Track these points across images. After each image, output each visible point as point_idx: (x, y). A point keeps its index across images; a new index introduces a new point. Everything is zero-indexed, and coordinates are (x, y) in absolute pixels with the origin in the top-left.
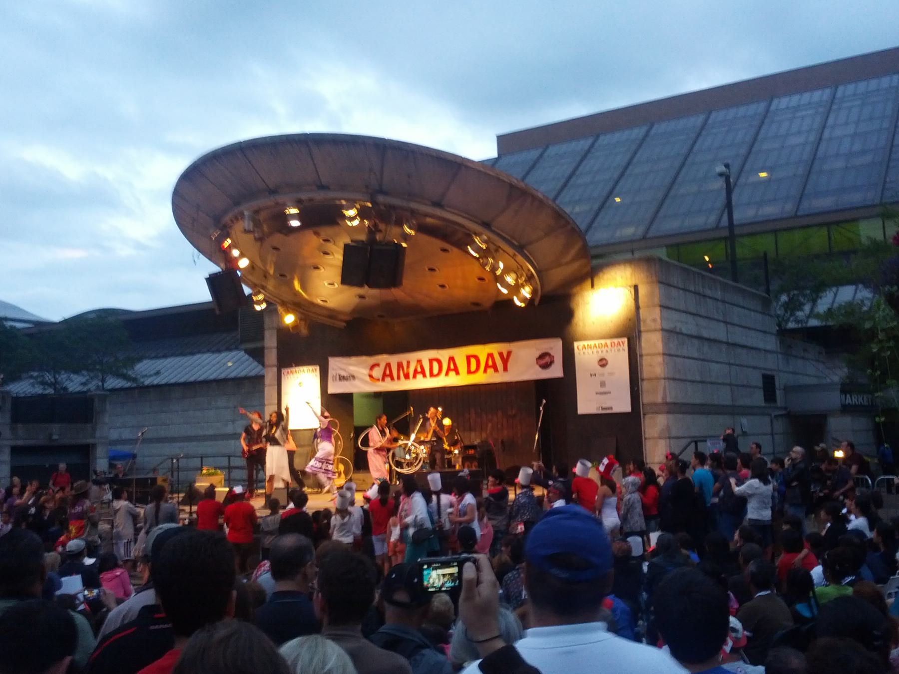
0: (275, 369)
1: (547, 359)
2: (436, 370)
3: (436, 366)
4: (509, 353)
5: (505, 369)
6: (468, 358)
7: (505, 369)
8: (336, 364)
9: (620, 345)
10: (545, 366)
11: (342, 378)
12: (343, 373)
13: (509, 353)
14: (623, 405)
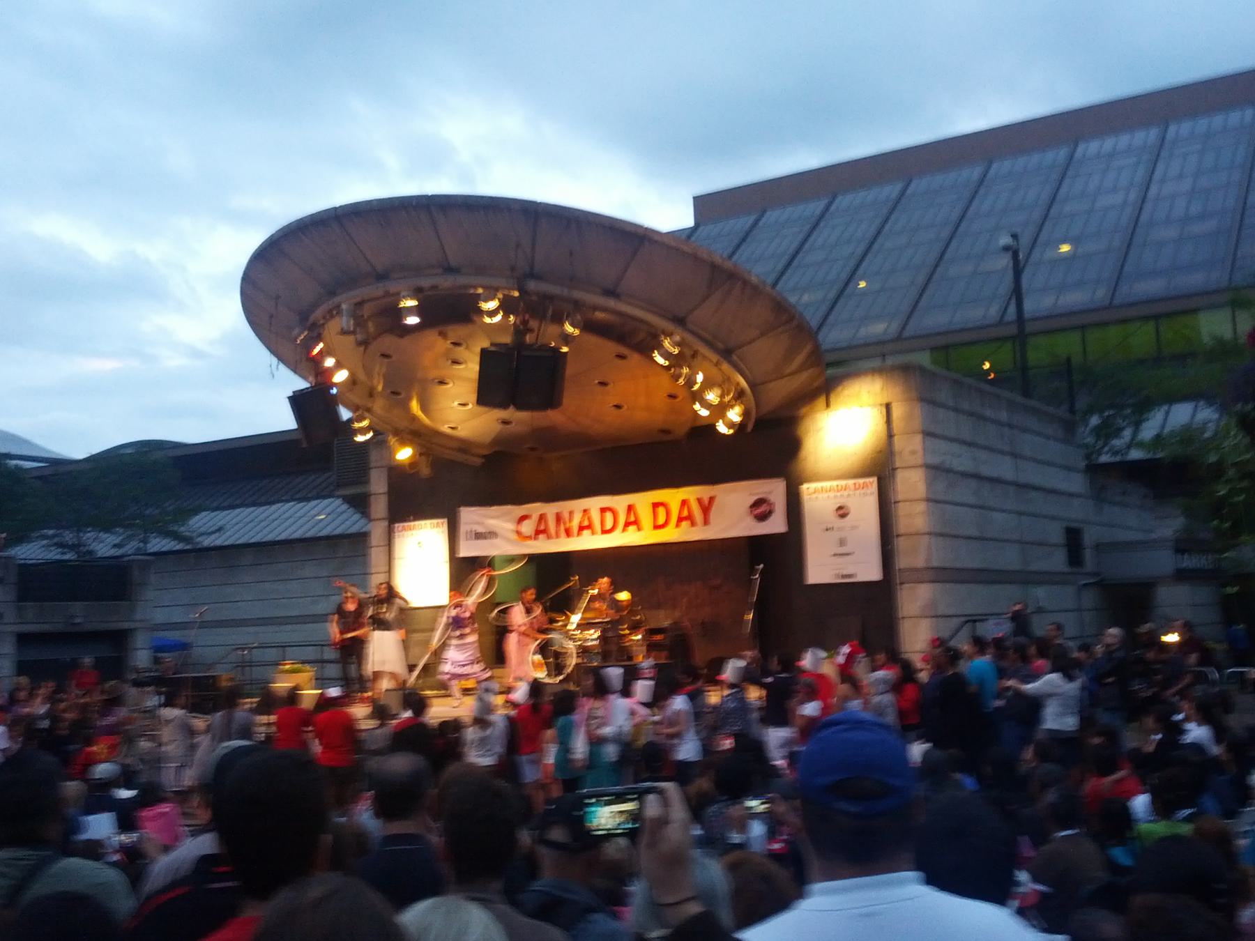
0: (386, 523)
1: (763, 509)
2: (609, 525)
3: (609, 517)
4: (712, 499)
5: (706, 522)
6: (656, 505)
7: (706, 522)
8: (470, 517)
9: (690, 518)
10: (762, 517)
11: (479, 536)
12: (480, 529)
13: (712, 499)
14: (870, 571)
